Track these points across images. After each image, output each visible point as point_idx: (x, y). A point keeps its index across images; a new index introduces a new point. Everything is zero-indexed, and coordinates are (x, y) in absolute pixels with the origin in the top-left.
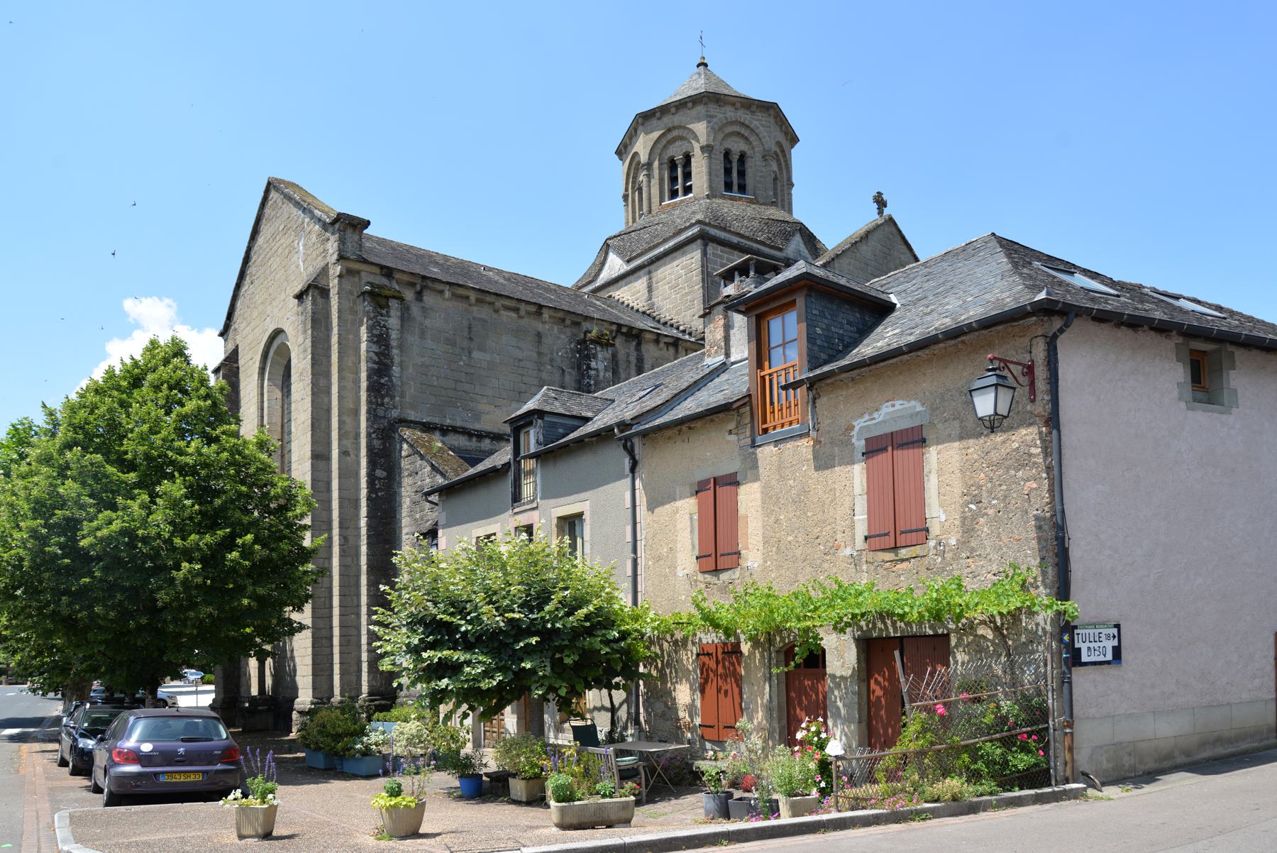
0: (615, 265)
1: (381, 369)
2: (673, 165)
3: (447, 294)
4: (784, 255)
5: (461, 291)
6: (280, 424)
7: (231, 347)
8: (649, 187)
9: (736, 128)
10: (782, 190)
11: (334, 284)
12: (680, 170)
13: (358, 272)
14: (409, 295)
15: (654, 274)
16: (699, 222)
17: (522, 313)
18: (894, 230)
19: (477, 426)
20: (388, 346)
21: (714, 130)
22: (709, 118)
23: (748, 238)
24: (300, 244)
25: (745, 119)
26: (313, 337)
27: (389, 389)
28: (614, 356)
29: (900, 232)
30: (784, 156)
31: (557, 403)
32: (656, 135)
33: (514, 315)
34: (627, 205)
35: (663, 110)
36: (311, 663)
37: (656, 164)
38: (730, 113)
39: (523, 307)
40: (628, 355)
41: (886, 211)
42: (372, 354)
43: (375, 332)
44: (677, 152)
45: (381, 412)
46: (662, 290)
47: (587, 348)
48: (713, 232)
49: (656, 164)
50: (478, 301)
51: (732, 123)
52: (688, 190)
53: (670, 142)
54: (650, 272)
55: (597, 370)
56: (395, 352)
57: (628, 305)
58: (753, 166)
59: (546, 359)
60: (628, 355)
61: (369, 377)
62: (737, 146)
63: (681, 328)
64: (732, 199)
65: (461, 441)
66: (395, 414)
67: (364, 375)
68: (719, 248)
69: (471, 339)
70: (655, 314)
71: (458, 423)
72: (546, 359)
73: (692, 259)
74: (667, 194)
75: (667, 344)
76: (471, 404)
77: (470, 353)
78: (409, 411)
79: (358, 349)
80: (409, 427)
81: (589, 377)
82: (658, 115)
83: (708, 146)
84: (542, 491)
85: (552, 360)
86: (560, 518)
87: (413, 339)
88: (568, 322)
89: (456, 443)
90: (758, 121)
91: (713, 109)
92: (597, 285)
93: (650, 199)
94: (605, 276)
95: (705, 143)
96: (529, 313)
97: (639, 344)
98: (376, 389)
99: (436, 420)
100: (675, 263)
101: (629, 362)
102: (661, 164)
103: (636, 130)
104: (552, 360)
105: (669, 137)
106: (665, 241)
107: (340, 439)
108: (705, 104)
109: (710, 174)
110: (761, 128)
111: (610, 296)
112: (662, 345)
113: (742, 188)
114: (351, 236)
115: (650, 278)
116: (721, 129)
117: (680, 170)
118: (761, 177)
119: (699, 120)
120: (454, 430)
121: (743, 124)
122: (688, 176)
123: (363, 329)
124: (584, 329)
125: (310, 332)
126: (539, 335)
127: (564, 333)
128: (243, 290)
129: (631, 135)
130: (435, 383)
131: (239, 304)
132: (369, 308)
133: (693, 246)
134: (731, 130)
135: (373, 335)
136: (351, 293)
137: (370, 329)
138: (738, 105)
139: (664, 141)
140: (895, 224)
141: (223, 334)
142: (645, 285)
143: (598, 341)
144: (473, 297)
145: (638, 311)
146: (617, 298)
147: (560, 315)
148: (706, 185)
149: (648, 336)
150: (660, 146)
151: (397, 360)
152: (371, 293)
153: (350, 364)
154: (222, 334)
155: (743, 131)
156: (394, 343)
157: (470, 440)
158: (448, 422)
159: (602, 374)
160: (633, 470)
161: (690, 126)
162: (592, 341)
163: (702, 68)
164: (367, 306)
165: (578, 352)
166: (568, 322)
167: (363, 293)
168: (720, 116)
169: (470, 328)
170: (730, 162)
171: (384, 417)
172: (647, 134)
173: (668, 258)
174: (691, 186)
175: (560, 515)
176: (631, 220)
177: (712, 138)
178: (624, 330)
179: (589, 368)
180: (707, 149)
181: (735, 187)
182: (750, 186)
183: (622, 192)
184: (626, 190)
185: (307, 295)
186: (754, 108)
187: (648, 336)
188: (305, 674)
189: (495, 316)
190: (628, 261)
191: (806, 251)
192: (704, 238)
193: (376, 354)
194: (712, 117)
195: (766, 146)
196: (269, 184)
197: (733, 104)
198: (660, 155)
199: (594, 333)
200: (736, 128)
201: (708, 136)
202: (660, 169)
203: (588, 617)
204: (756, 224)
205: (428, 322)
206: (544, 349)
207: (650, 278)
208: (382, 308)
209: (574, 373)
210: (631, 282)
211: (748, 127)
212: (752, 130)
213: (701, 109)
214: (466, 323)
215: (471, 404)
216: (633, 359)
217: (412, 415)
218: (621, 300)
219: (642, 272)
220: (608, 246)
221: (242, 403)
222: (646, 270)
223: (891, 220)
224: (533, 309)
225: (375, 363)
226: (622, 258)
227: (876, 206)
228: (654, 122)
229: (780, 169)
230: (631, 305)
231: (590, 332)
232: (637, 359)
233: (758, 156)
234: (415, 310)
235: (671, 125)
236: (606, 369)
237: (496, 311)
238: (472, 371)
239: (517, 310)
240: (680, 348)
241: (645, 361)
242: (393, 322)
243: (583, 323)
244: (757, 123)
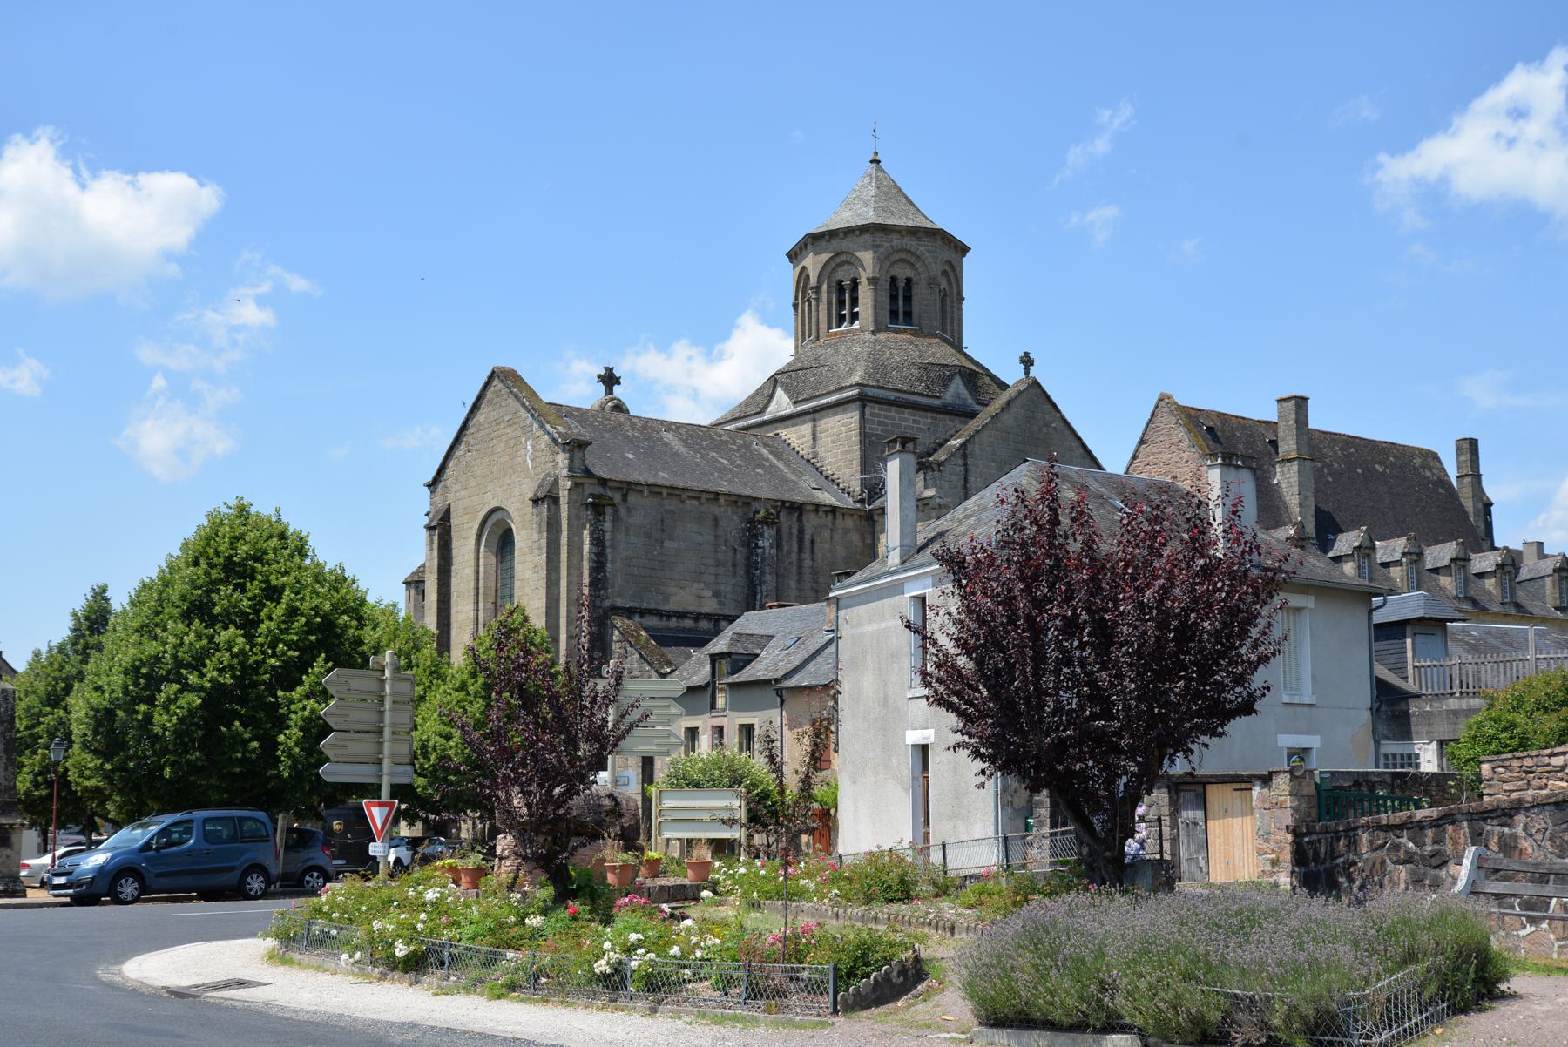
0: (782, 403)
1: (598, 566)
2: (840, 288)
3: (646, 493)
4: (943, 401)
5: (657, 490)
6: (494, 588)
7: (442, 505)
8: (818, 311)
9: (903, 255)
10: (952, 307)
11: (564, 496)
12: (847, 296)
13: (582, 484)
14: (617, 498)
15: (818, 423)
16: (858, 385)
17: (703, 500)
18: (1039, 391)
19: (667, 607)
20: (604, 547)
21: (880, 261)
22: (875, 247)
23: (905, 392)
24: (528, 443)
26: (548, 538)
27: (604, 583)
28: (778, 531)
29: (1045, 392)
30: (954, 270)
31: (739, 645)
32: (825, 257)
33: (695, 502)
34: (796, 315)
35: (832, 234)
37: (824, 287)
38: (896, 241)
39: (703, 496)
40: (790, 527)
41: (1034, 372)
42: (593, 555)
43: (595, 536)
44: (844, 275)
45: (598, 604)
46: (825, 441)
47: (755, 528)
48: (870, 392)
49: (824, 287)
50: (668, 494)
51: (898, 251)
52: (854, 317)
53: (834, 270)
54: (814, 420)
55: (763, 548)
56: (609, 550)
57: (794, 449)
58: (920, 293)
59: (721, 541)
60: (790, 527)
61: (590, 575)
62: (902, 272)
63: (841, 486)
64: (898, 332)
65: (653, 621)
66: (608, 603)
67: (586, 572)
68: (877, 406)
69: (663, 531)
70: (818, 465)
71: (653, 606)
72: (721, 541)
73: (851, 419)
74: (834, 320)
75: (826, 512)
76: (663, 588)
77: (662, 543)
78: (616, 599)
79: (581, 550)
80: (618, 615)
81: (757, 555)
82: (827, 237)
83: (874, 278)
84: (730, 704)
85: (726, 541)
86: (740, 725)
87: (620, 536)
88: (740, 504)
89: (650, 623)
90: (922, 247)
91: (880, 238)
92: (765, 418)
93: (818, 325)
94: (773, 411)
95: (871, 276)
96: (708, 499)
97: (800, 515)
98: (595, 584)
99: (637, 605)
100: (837, 418)
101: (791, 534)
102: (829, 287)
103: (806, 245)
104: (726, 541)
105: (838, 260)
106: (829, 393)
107: (568, 626)
108: (872, 234)
109: (875, 307)
110: (927, 254)
111: (777, 434)
112: (821, 514)
113: (908, 315)
114: (578, 454)
115: (815, 426)
116: (887, 258)
117: (847, 296)
118: (926, 305)
119: (866, 248)
120: (651, 612)
121: (909, 251)
122: (854, 301)
123: (586, 534)
124: (754, 510)
125: (545, 534)
126: (716, 520)
127: (736, 513)
128: (457, 454)
130: (636, 573)
131: (451, 464)
132: (591, 517)
133: (853, 406)
134: (897, 258)
135: (594, 539)
136: (576, 501)
137: (591, 534)
138: (904, 233)
139: (833, 264)
141: (433, 485)
142: (810, 431)
143: (765, 522)
144: (665, 492)
145: (802, 457)
146: (784, 438)
147: (733, 498)
148: (871, 319)
149: (808, 507)
150: (829, 269)
151: (610, 557)
152: (592, 504)
153: (575, 562)
154: (428, 486)
155: (909, 257)
156: (608, 544)
157: (661, 620)
158: (645, 605)
159: (767, 551)
160: (781, 705)
161: (858, 254)
162: (760, 522)
163: (874, 165)
164: (589, 515)
165: (748, 531)
166: (740, 504)
167: (587, 504)
168: (886, 245)
169: (662, 521)
170: (897, 289)
171: (600, 607)
172: (816, 254)
173: (831, 411)
174: (857, 313)
177: (877, 269)
178: (787, 505)
179: (757, 546)
180: (873, 281)
181: (901, 317)
182: (915, 316)
183: (791, 299)
184: (796, 298)
185: (543, 502)
186: (919, 234)
187: (808, 507)
189: (681, 506)
190: (795, 403)
191: (966, 392)
192: (863, 400)
193: (595, 554)
194: (878, 246)
195: (932, 274)
196: (493, 372)
197: (900, 232)
198: (829, 277)
199: (762, 513)
200: (903, 255)
201: (874, 267)
202: (829, 292)
203: (757, 794)
204: (915, 371)
205: (631, 521)
206: (720, 532)
207: (815, 426)
208: (600, 515)
209: (744, 550)
210: (796, 425)
212: (918, 257)
213: (867, 237)
214: (659, 516)
215: (663, 588)
216: (795, 532)
217: (619, 602)
218: (788, 441)
219: (807, 418)
220: (776, 380)
221: (454, 561)
222: (812, 416)
223: (1036, 384)
224: (712, 496)
225: (595, 562)
226: (790, 397)
227: (1022, 366)
228: (823, 243)
229: (950, 284)
230: (797, 449)
231: (758, 512)
232: (799, 530)
233: (924, 284)
234: (622, 512)
235: (839, 250)
236: (771, 547)
237: (682, 502)
238: (664, 559)
239: (698, 498)
240: (837, 514)
241: (806, 532)
242: (608, 526)
243: (752, 504)
244: (923, 249)
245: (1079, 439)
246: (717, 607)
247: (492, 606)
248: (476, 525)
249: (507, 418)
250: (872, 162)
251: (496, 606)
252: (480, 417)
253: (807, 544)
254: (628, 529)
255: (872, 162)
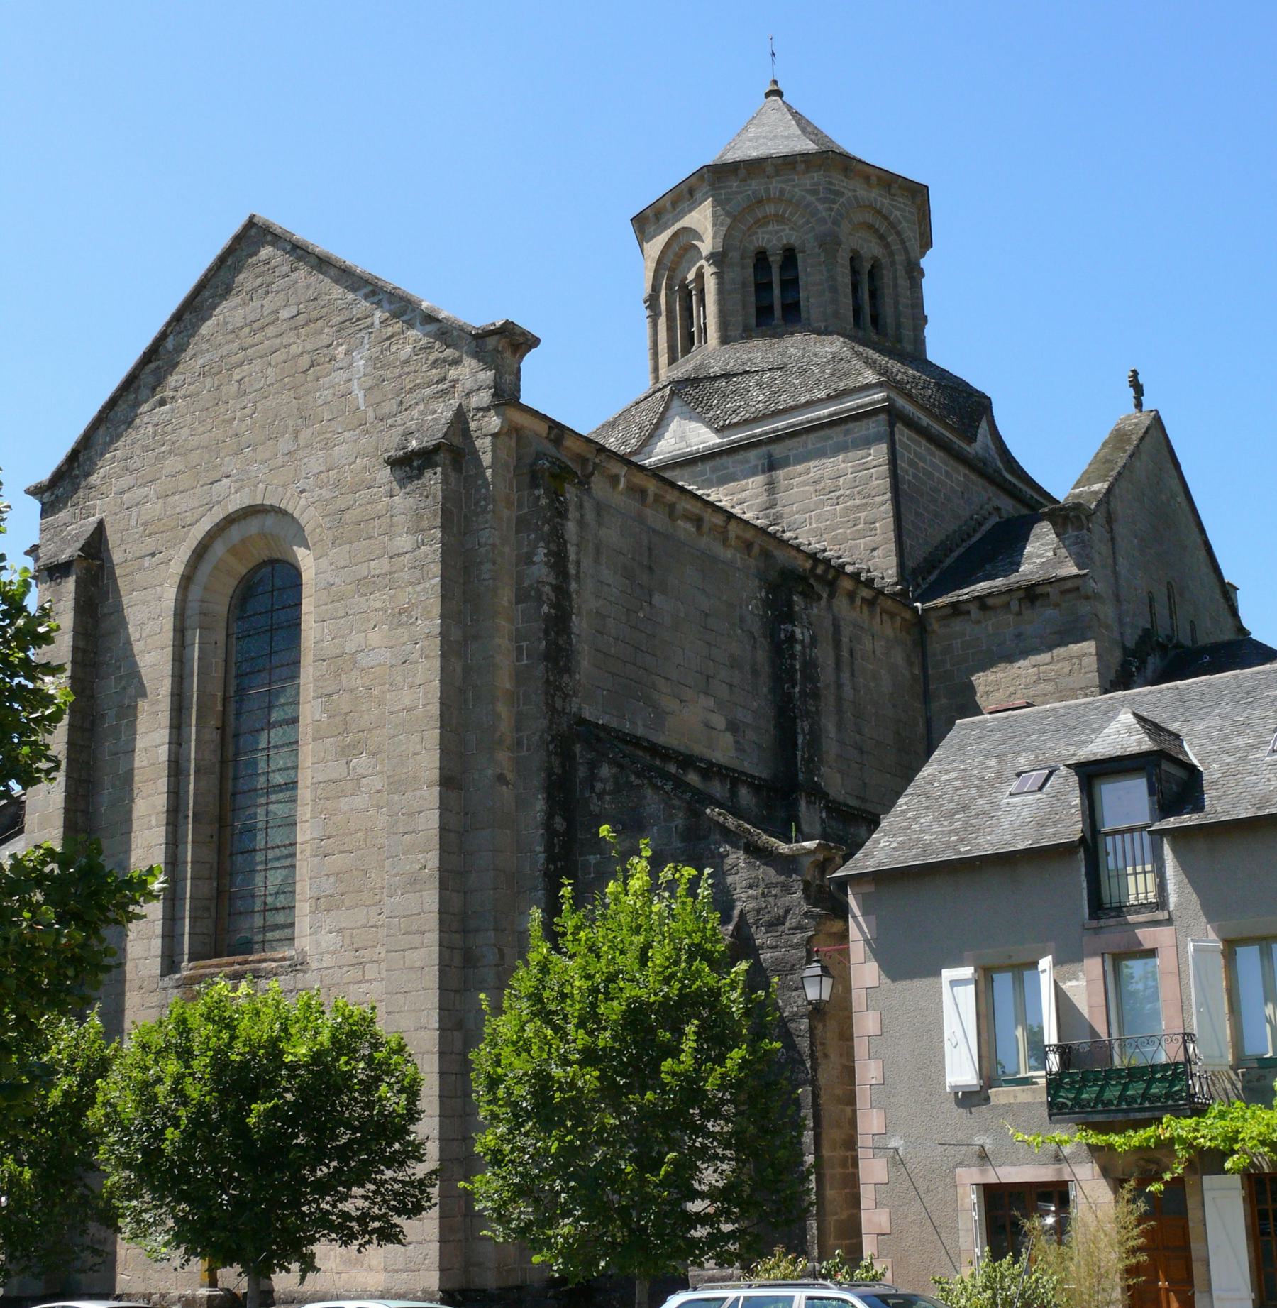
25: (883, 204)
36: (436, 906)
99: (614, 724)
103: (691, 192)
110: (905, 224)
129: (683, 196)
140: (1208, 1265)
175: (1161, 414)
176: (663, 359)
183: (646, 289)
188: (426, 928)
197: (867, 178)
211: (886, 218)
219: (752, 455)
244: (898, 213)
245: (1202, 531)
246: (732, 753)
247: (216, 736)
248: (184, 553)
249: (284, 314)
250: (768, 95)
251: (223, 738)
252: (229, 313)
253: (845, 654)
254: (598, 551)
255: (768, 95)
